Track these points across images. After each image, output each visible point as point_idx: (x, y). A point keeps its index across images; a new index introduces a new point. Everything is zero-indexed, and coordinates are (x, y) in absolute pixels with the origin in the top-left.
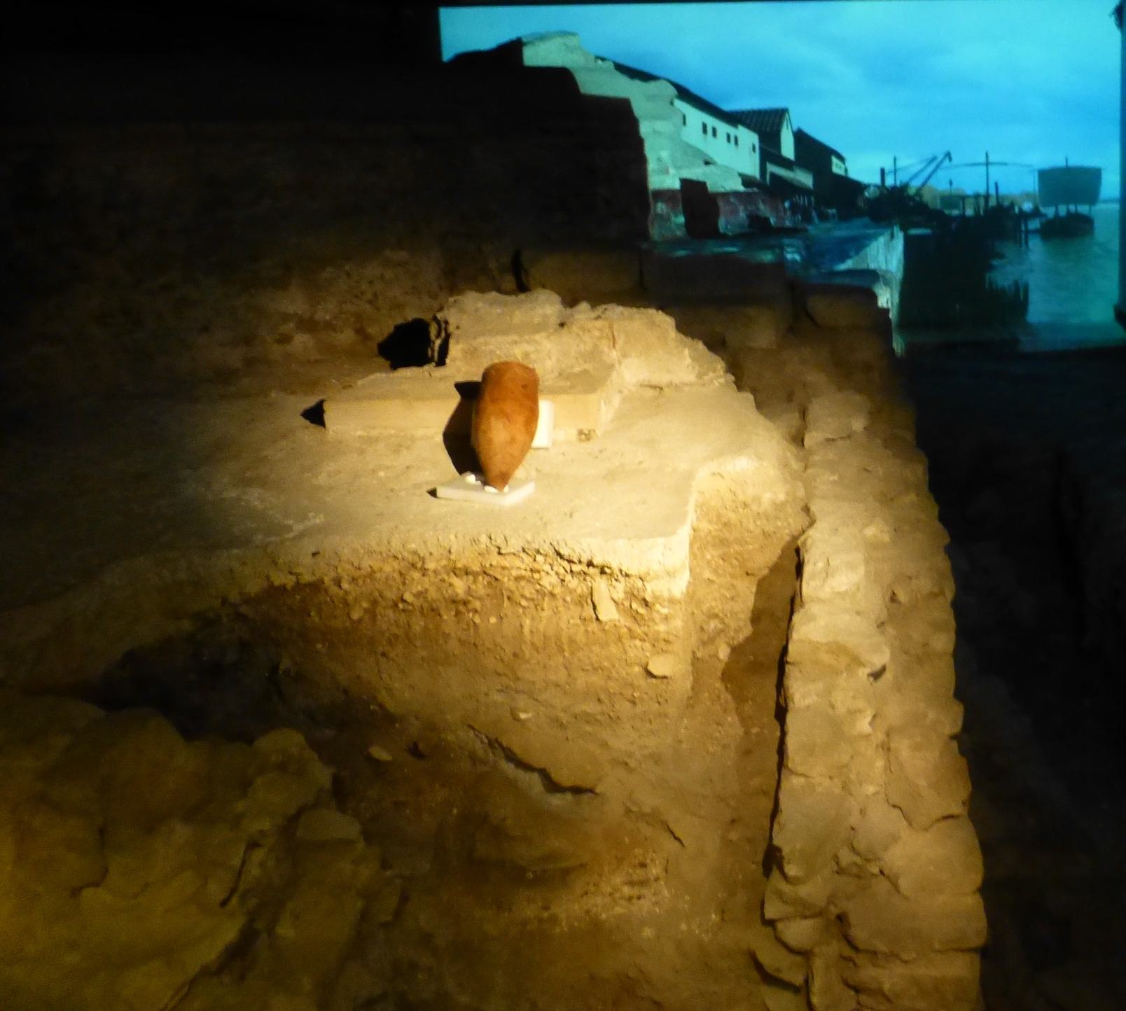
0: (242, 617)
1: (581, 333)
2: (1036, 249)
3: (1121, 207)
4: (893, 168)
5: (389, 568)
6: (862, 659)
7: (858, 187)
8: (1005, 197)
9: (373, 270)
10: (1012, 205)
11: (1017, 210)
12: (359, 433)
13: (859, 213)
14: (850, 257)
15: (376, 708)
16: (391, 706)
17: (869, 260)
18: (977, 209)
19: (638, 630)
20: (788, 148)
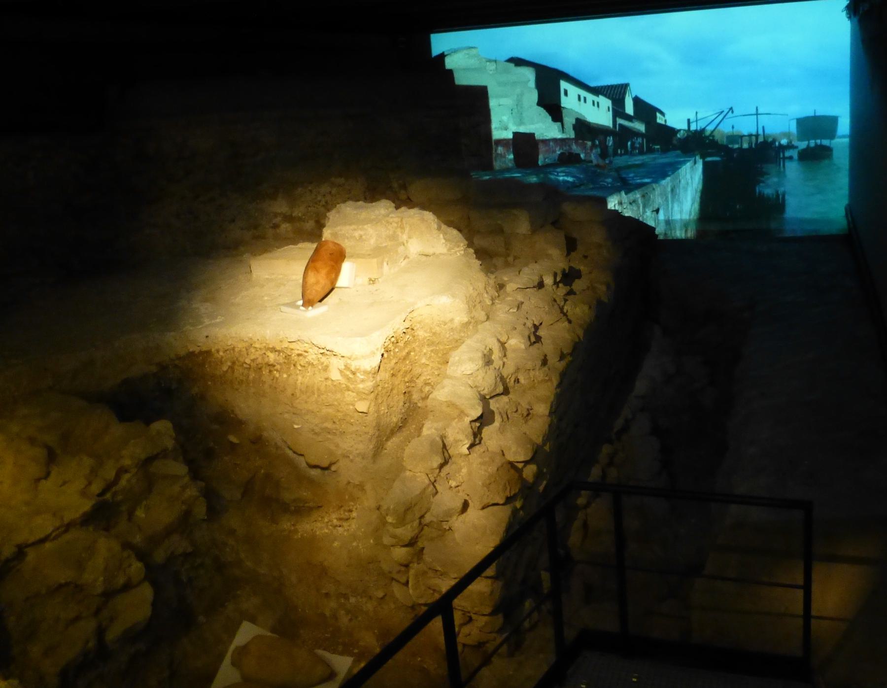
0: (176, 366)
1: (387, 225)
2: (793, 170)
3: (850, 140)
4: (695, 119)
5: (241, 346)
6: (466, 412)
7: (673, 131)
8: (769, 136)
9: (325, 188)
10: (774, 141)
11: (777, 144)
12: (267, 277)
13: (675, 148)
14: (669, 176)
15: (234, 416)
16: (240, 417)
17: (681, 177)
18: (750, 143)
19: (351, 387)
20: (629, 109)
